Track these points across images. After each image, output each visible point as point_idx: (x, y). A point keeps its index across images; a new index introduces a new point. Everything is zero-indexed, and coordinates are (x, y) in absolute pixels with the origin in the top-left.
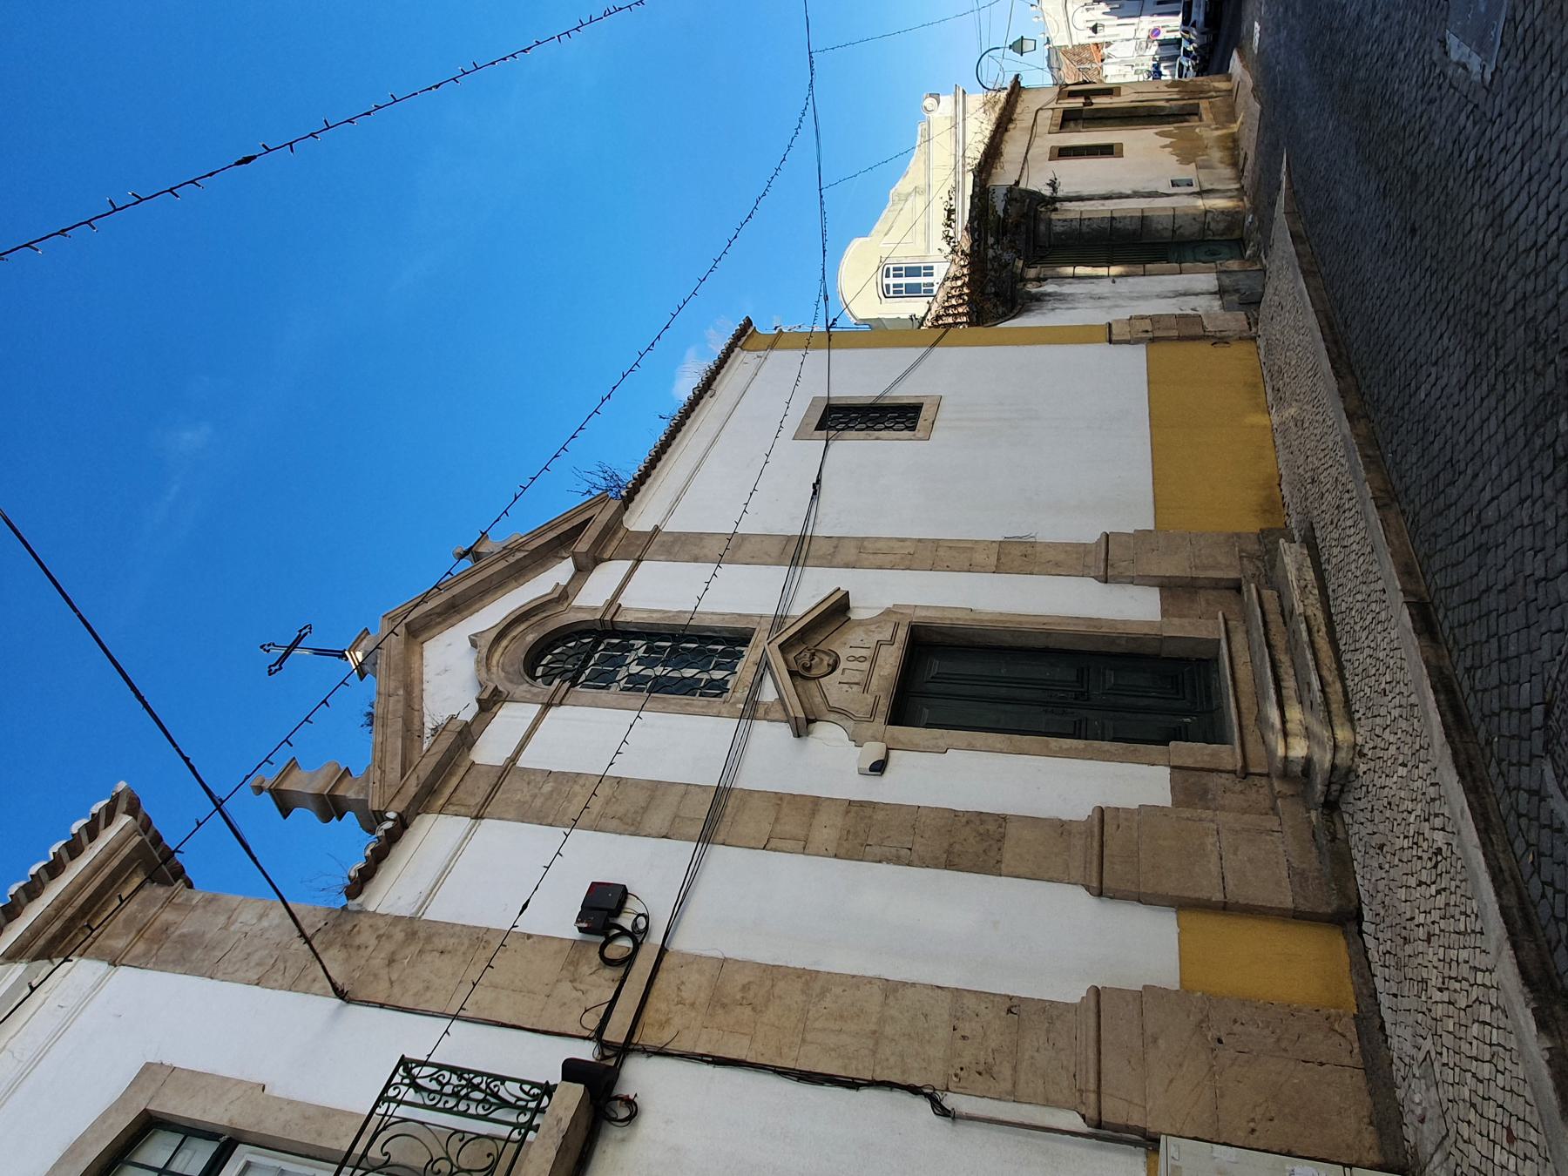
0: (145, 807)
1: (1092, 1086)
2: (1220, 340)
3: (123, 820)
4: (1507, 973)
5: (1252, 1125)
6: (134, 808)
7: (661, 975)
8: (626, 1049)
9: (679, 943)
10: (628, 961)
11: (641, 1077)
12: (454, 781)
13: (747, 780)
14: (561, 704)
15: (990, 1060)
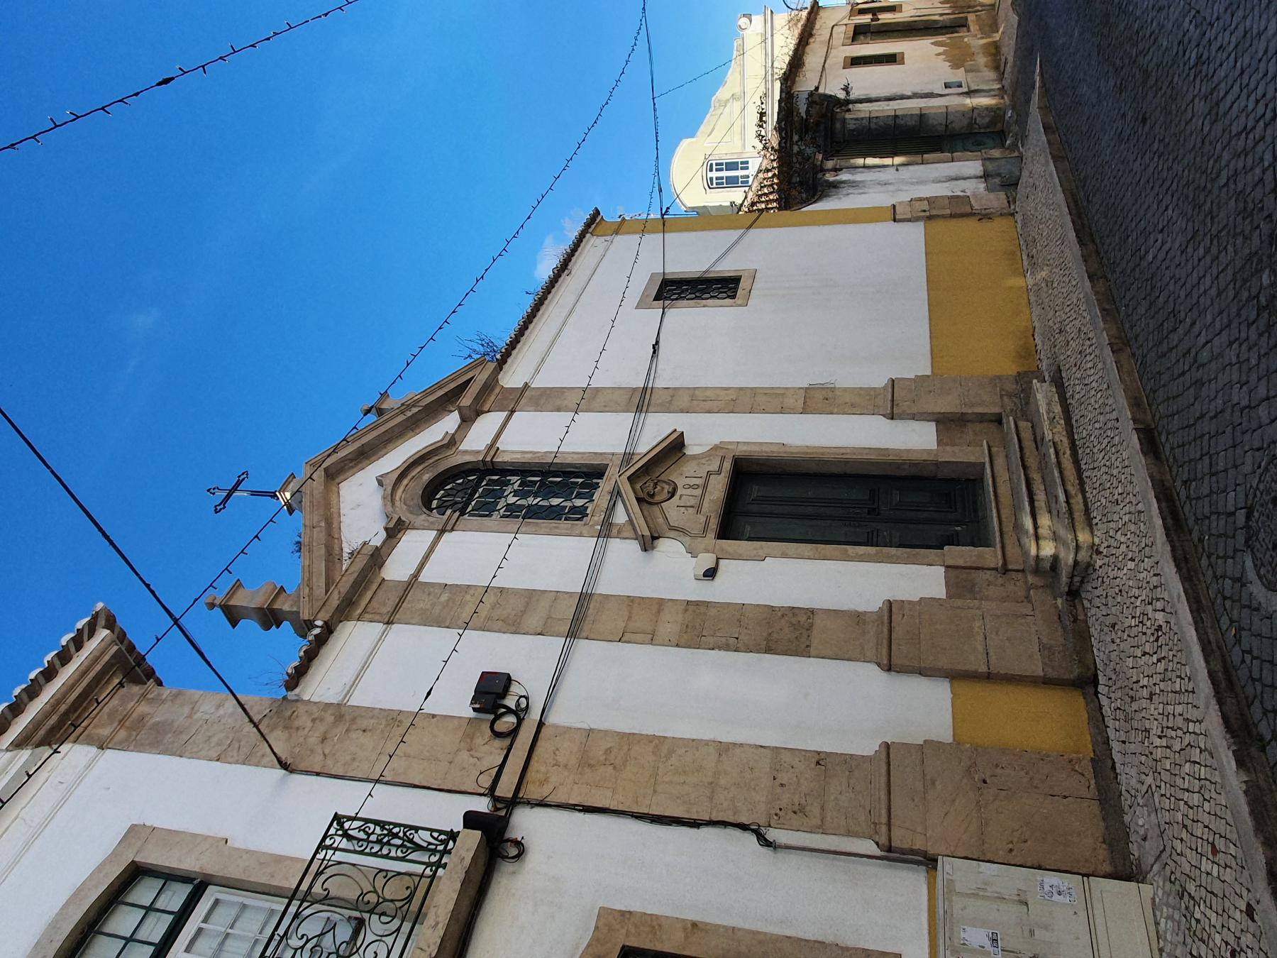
0: (121, 623)
1: (884, 820)
3: (103, 633)
8: (514, 802)
10: (514, 733)
11: (525, 823)
12: (369, 594)
13: (602, 588)
14: (452, 530)
15: (803, 801)
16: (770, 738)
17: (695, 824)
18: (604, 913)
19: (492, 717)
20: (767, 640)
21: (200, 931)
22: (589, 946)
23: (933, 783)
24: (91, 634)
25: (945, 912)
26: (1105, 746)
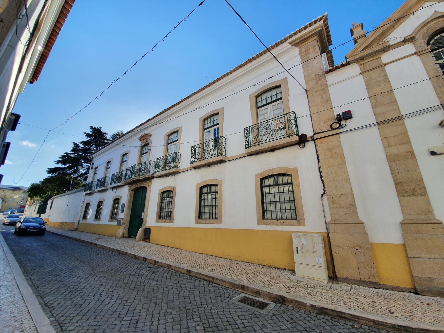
0: (329, 21)
1: (335, 222)
3: (322, 22)
4: (340, 309)
6: (326, 19)
8: (314, 140)
11: (310, 145)
12: (372, 59)
13: (408, 122)
14: (419, 56)
16: (355, 191)
17: (322, 180)
20: (401, 183)
23: (352, 236)
24: (320, 21)
26: (385, 288)
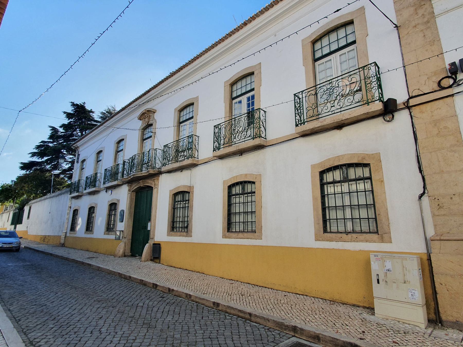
1: (442, 238)
2: (30, 207)
5: (444, 284)
7: (441, 101)
9: (456, 98)
10: (443, 88)
11: (402, 117)
15: (445, 207)
18: (378, 155)
19: (450, 75)
21: (323, 63)
22: (367, 154)
25: (394, 256)
